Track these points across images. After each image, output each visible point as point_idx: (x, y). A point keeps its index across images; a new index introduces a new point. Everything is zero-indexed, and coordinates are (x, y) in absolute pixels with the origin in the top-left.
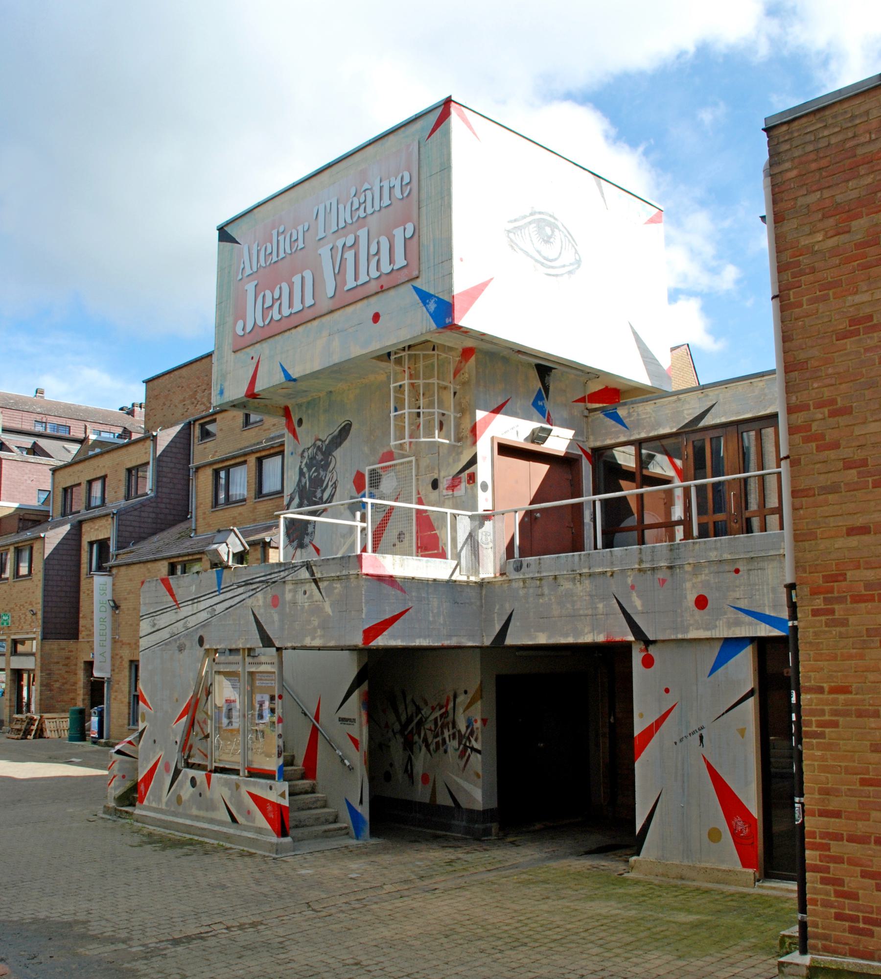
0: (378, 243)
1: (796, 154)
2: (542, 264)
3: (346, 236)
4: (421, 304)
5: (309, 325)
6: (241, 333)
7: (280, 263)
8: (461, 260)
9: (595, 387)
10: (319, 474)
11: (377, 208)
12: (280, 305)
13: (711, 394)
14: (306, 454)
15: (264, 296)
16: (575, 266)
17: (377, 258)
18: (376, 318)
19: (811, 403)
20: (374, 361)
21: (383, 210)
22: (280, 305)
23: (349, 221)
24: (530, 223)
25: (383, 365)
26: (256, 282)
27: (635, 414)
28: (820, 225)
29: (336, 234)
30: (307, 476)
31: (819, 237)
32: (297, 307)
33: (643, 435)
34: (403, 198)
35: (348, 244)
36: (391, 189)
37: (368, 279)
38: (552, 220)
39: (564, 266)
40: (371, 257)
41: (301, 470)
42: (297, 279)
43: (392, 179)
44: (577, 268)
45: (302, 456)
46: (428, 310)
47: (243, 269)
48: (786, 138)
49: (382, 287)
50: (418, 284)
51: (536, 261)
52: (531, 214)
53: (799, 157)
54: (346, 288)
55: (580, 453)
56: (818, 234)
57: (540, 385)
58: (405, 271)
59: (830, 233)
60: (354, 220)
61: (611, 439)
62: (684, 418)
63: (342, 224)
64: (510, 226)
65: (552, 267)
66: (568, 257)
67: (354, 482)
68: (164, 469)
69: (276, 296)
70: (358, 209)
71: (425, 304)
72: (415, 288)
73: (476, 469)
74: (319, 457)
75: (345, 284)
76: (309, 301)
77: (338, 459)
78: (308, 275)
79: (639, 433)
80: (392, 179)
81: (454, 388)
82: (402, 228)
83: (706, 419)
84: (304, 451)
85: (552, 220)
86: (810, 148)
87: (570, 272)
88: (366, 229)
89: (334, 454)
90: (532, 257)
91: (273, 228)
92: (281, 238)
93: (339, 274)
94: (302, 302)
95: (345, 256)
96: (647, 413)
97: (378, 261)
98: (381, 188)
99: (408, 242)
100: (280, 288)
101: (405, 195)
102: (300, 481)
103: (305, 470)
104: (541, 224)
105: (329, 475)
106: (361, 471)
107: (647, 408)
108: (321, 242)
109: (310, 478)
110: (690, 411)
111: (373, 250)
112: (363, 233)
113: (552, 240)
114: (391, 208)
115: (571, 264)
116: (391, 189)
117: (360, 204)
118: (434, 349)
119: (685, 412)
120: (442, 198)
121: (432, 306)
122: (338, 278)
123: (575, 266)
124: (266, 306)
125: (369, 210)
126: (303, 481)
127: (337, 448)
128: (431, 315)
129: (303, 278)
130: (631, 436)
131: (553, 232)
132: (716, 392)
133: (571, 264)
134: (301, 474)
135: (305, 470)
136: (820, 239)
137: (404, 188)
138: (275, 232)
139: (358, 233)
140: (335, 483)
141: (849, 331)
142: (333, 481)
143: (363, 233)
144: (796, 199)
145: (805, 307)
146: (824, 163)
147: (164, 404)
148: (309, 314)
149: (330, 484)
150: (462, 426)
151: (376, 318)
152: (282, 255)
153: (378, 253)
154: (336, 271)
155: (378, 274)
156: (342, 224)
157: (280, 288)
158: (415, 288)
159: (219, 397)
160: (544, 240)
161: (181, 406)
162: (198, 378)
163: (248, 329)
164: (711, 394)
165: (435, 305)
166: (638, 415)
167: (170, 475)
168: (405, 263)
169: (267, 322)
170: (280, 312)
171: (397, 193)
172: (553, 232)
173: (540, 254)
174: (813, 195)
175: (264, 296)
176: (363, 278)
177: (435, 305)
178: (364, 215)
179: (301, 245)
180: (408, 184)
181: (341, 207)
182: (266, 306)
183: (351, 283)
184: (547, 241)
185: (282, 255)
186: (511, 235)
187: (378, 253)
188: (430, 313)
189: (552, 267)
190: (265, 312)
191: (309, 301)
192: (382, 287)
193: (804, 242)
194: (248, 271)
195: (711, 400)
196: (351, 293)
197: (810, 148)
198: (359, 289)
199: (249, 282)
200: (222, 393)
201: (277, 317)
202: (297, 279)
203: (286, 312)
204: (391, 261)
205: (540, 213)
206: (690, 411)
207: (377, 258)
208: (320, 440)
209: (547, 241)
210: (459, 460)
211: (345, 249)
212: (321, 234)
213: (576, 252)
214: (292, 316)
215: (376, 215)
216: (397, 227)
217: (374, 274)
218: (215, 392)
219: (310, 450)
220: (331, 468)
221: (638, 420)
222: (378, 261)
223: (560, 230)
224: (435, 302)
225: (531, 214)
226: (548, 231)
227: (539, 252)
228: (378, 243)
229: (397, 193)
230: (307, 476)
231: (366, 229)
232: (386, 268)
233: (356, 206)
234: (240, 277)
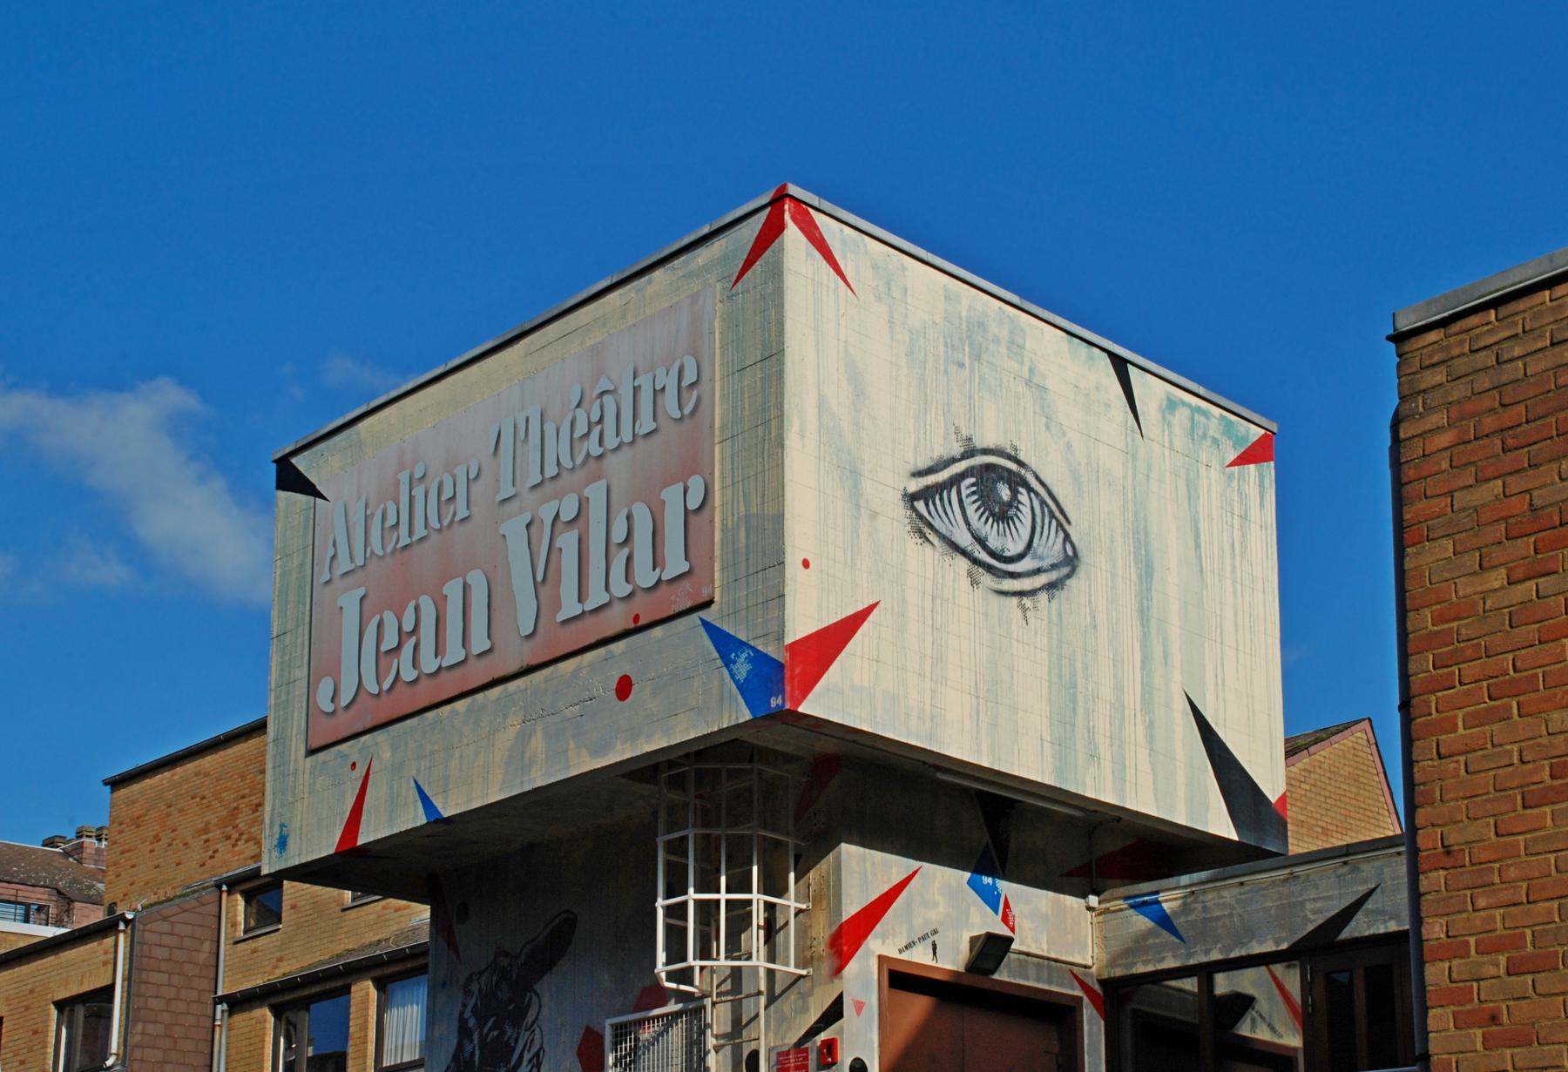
0: (629, 517)
1: (1455, 396)
2: (989, 568)
3: (560, 496)
4: (719, 662)
5: (480, 697)
6: (330, 708)
7: (416, 550)
8: (806, 564)
9: (1109, 845)
10: (503, 1032)
11: (627, 437)
12: (416, 647)
13: (1365, 867)
14: (475, 988)
15: (380, 625)
16: (1065, 570)
17: (626, 551)
18: (624, 688)
19: (1472, 940)
20: (624, 781)
21: (640, 442)
22: (416, 647)
23: (567, 462)
24: (956, 480)
25: (644, 789)
26: (361, 592)
27: (1199, 906)
28: (1498, 555)
29: (540, 491)
30: (476, 1037)
31: (1497, 579)
32: (454, 654)
33: (1216, 956)
34: (681, 419)
35: (566, 516)
36: (658, 393)
37: (605, 599)
38: (1013, 466)
39: (1038, 571)
40: (613, 549)
41: (463, 1022)
42: (453, 590)
43: (661, 371)
44: (1069, 576)
45: (467, 992)
46: (733, 676)
47: (333, 558)
48: (1436, 359)
49: (636, 618)
50: (708, 615)
51: (976, 561)
52: (969, 453)
53: (1459, 402)
54: (561, 617)
55: (1078, 992)
56: (1494, 574)
57: (987, 839)
58: (686, 584)
59: (1519, 574)
60: (579, 460)
61: (1146, 962)
62: (1306, 920)
63: (551, 470)
64: (914, 486)
65: (1013, 575)
66: (1050, 547)
67: (580, 1053)
68: (152, 1003)
69: (408, 626)
70: (586, 436)
71: (728, 663)
72: (705, 624)
73: (841, 1031)
74: (504, 994)
75: (558, 606)
76: (479, 643)
77: (545, 1000)
78: (477, 580)
79: (1207, 952)
80: (661, 371)
81: (797, 846)
82: (681, 485)
83: (1353, 923)
84: (469, 980)
85: (1013, 466)
86: (1483, 382)
87: (1051, 586)
88: (602, 484)
89: (537, 987)
90: (964, 553)
91: (401, 467)
92: (418, 492)
93: (545, 581)
94: (465, 642)
95: (558, 543)
96: (1224, 906)
97: (629, 559)
98: (636, 390)
99: (692, 519)
100: (417, 608)
101: (687, 411)
102: (460, 1047)
103: (472, 1022)
104: (987, 476)
105: (525, 1036)
106: (596, 1028)
107: (1225, 893)
108: (507, 508)
109: (482, 1040)
110: (1319, 905)
111: (619, 535)
112: (595, 493)
113: (1012, 512)
114: (657, 438)
115: (1054, 567)
116: (658, 393)
117: (590, 426)
118: (751, 760)
119: (1309, 906)
120: (766, 423)
121: (743, 668)
122: (543, 592)
123: (1065, 570)
124: (384, 648)
125: (611, 441)
126: (468, 1048)
127: (543, 974)
128: (739, 687)
129: (466, 587)
130: (1190, 955)
131: (1015, 493)
132: (1377, 864)
133: (1054, 567)
134: (464, 1032)
135: (472, 1022)
136: (1497, 584)
137: (684, 394)
138: (404, 478)
139: (587, 492)
140: (537, 1055)
141: (1551, 788)
142: (534, 1049)
143: (595, 493)
144: (1451, 494)
145: (1461, 730)
146: (1508, 417)
147: (157, 839)
148: (479, 673)
149: (527, 1056)
150: (814, 932)
151: (624, 688)
152: (420, 531)
153: (628, 540)
154: (539, 578)
155: (628, 589)
156: (551, 470)
157: (417, 608)
158: (705, 624)
159: (275, 854)
160: (993, 514)
161: (197, 844)
162: (242, 777)
163: (345, 699)
164: (1365, 867)
165: (748, 667)
166: (1205, 909)
167: (166, 1018)
168: (685, 567)
169: (386, 686)
170: (415, 664)
171: (670, 401)
172: (1015, 493)
173: (985, 547)
174: (1485, 486)
175: (380, 625)
176: (596, 597)
177: (748, 667)
178: (599, 451)
179: (462, 513)
180: (692, 385)
181: (550, 429)
182: (384, 648)
183: (571, 608)
184: (1003, 515)
185: (420, 531)
186: (920, 505)
187: (628, 540)
188: (736, 682)
189: (1013, 575)
190: (383, 660)
191: (479, 643)
192: (636, 618)
193: (1466, 588)
194: (344, 565)
195: (1366, 881)
196: (572, 627)
197: (1483, 382)
198: (589, 620)
199: (347, 590)
200: (282, 844)
201: (408, 674)
202: (453, 590)
203: (429, 664)
204: (657, 561)
205: (986, 452)
206: (1319, 905)
207: (626, 551)
208: (506, 954)
209: (1003, 515)
210: (805, 1010)
211: (559, 526)
212: (507, 491)
213: (1067, 537)
214: (444, 676)
215: (626, 452)
216: (668, 483)
217: (621, 588)
218: (268, 843)
219: (484, 978)
220: (529, 1019)
221: (1205, 920)
222: (629, 559)
223: (1030, 489)
224: (749, 660)
225: (964, 457)
226: (1005, 493)
227: (981, 541)
228: (629, 517)
229: (670, 401)
230: (476, 1037)
231: (602, 484)
232: (645, 576)
233: (581, 428)
234: (326, 577)
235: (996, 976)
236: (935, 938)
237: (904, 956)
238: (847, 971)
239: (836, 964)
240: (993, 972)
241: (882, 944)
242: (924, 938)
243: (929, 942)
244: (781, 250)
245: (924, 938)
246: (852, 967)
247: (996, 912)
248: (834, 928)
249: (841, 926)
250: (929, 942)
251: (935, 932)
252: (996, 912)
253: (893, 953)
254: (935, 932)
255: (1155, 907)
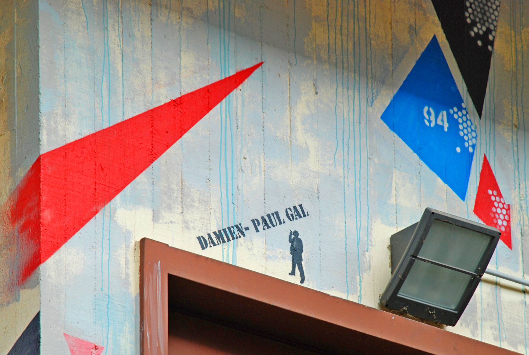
57: (434, 29)
235: (459, 329)
236: (297, 225)
237: (214, 253)
238: (49, 268)
239: (26, 253)
240: (452, 319)
241: (134, 217)
242: (268, 222)
243: (281, 233)
244: (39, 274)
245: (268, 222)
246: (68, 263)
247: (462, 195)
248: (22, 173)
249: (40, 156)
250: (281, 233)
251: (299, 213)
252: (462, 195)
253: (182, 239)
254: (299, 213)
255: (46, 171)
